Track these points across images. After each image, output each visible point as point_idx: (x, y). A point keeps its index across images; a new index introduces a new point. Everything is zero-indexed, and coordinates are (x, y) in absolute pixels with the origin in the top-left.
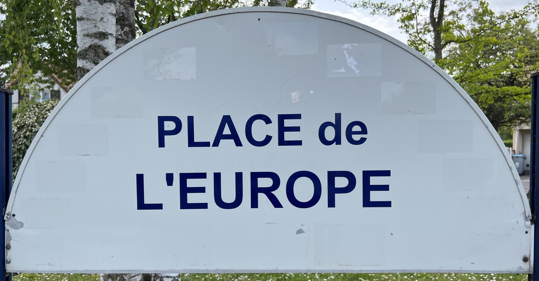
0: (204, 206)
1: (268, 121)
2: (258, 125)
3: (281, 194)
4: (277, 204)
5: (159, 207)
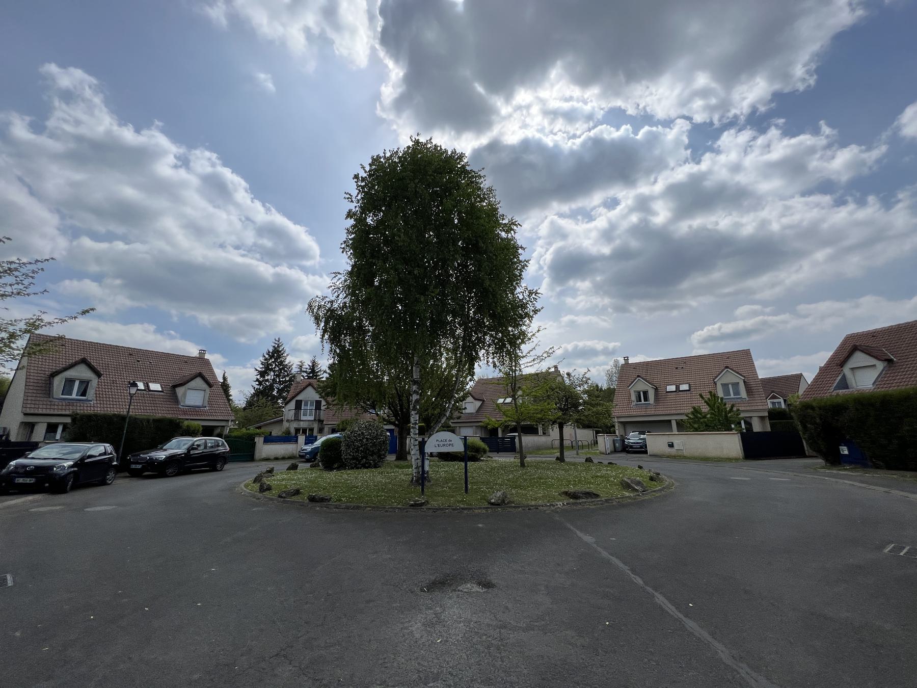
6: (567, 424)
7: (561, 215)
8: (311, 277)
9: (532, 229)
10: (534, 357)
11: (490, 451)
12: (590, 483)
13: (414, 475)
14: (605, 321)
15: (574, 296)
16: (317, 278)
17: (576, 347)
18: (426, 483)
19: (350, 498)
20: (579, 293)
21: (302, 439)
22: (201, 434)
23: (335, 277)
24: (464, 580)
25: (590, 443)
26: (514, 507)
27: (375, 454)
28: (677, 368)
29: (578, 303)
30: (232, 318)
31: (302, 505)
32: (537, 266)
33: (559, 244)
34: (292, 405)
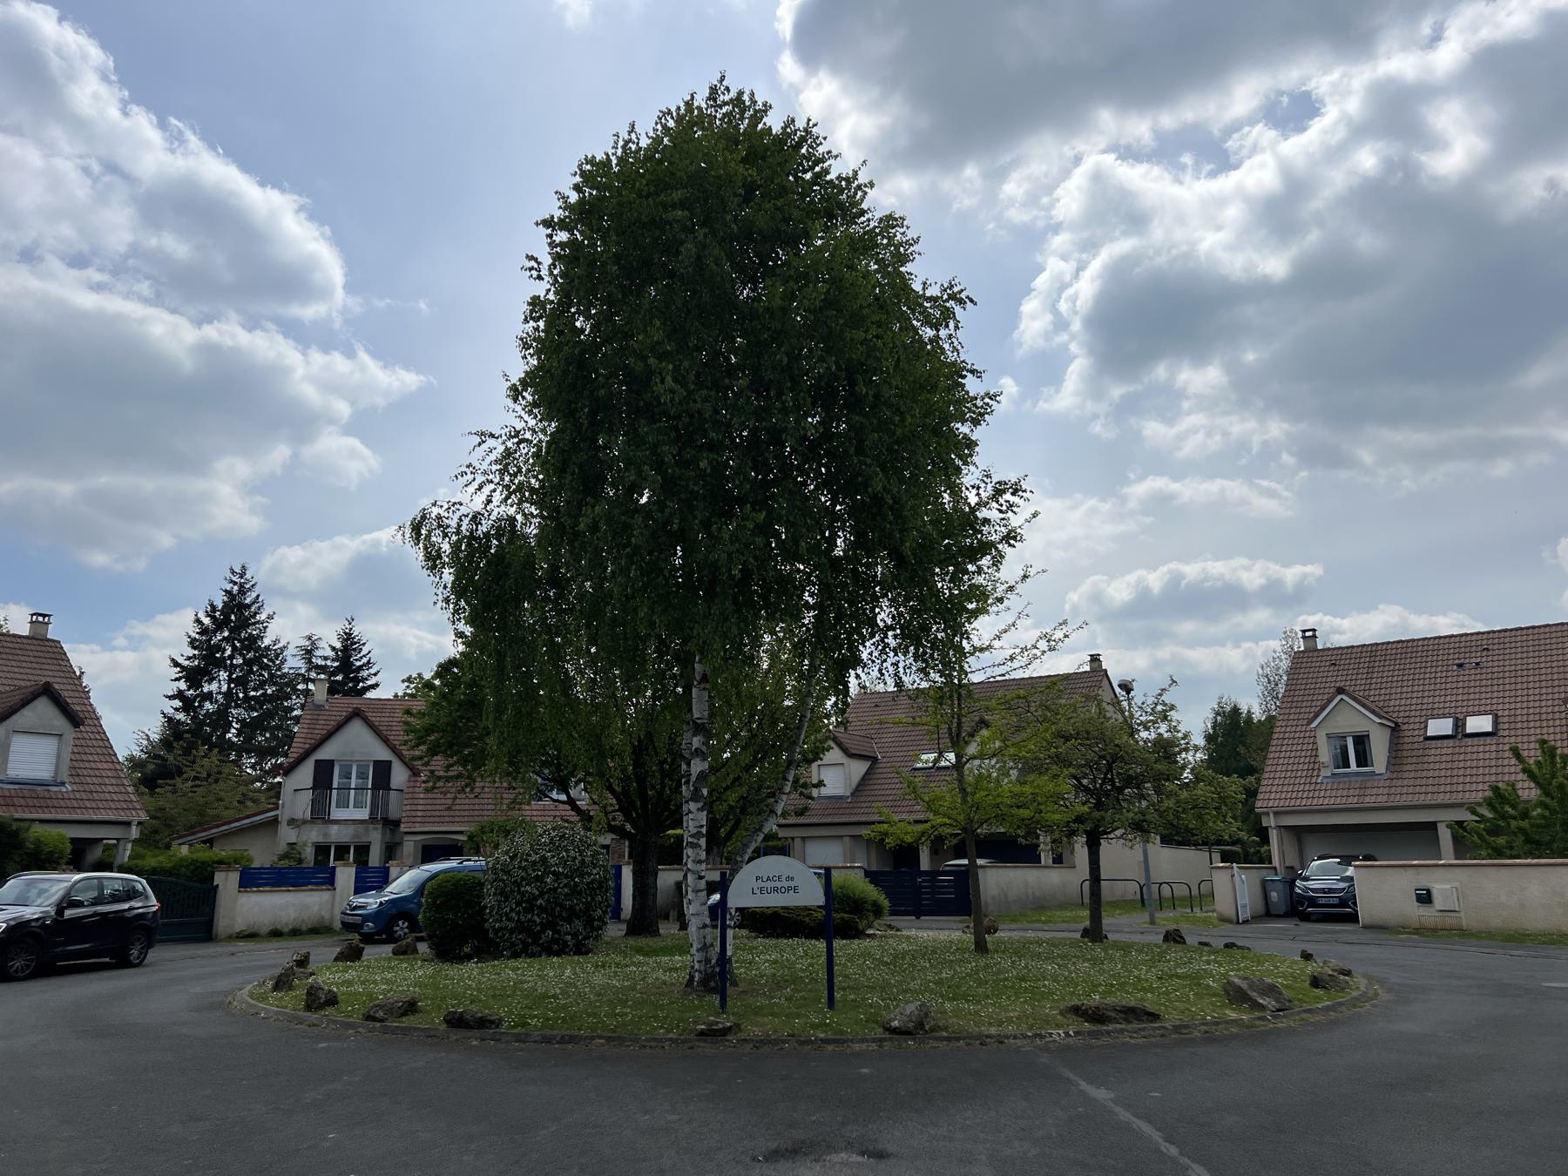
6: (1112, 836)
7: (1129, 153)
8: (317, 358)
9: (1032, 200)
10: (1012, 651)
11: (893, 913)
12: (1151, 990)
13: (697, 966)
14: (1271, 494)
15: (1169, 415)
16: (339, 363)
17: (1175, 580)
18: (730, 991)
19: (548, 1019)
20: (1186, 405)
21: (346, 875)
22: (67, 863)
23: (480, 445)
24: (832, 1148)
25: (1195, 892)
26: (948, 1039)
27: (579, 918)
28: (1460, 666)
29: (1182, 438)
30: (65, 489)
31: (430, 1034)
32: (1049, 317)
33: (1123, 246)
34: (305, 775)
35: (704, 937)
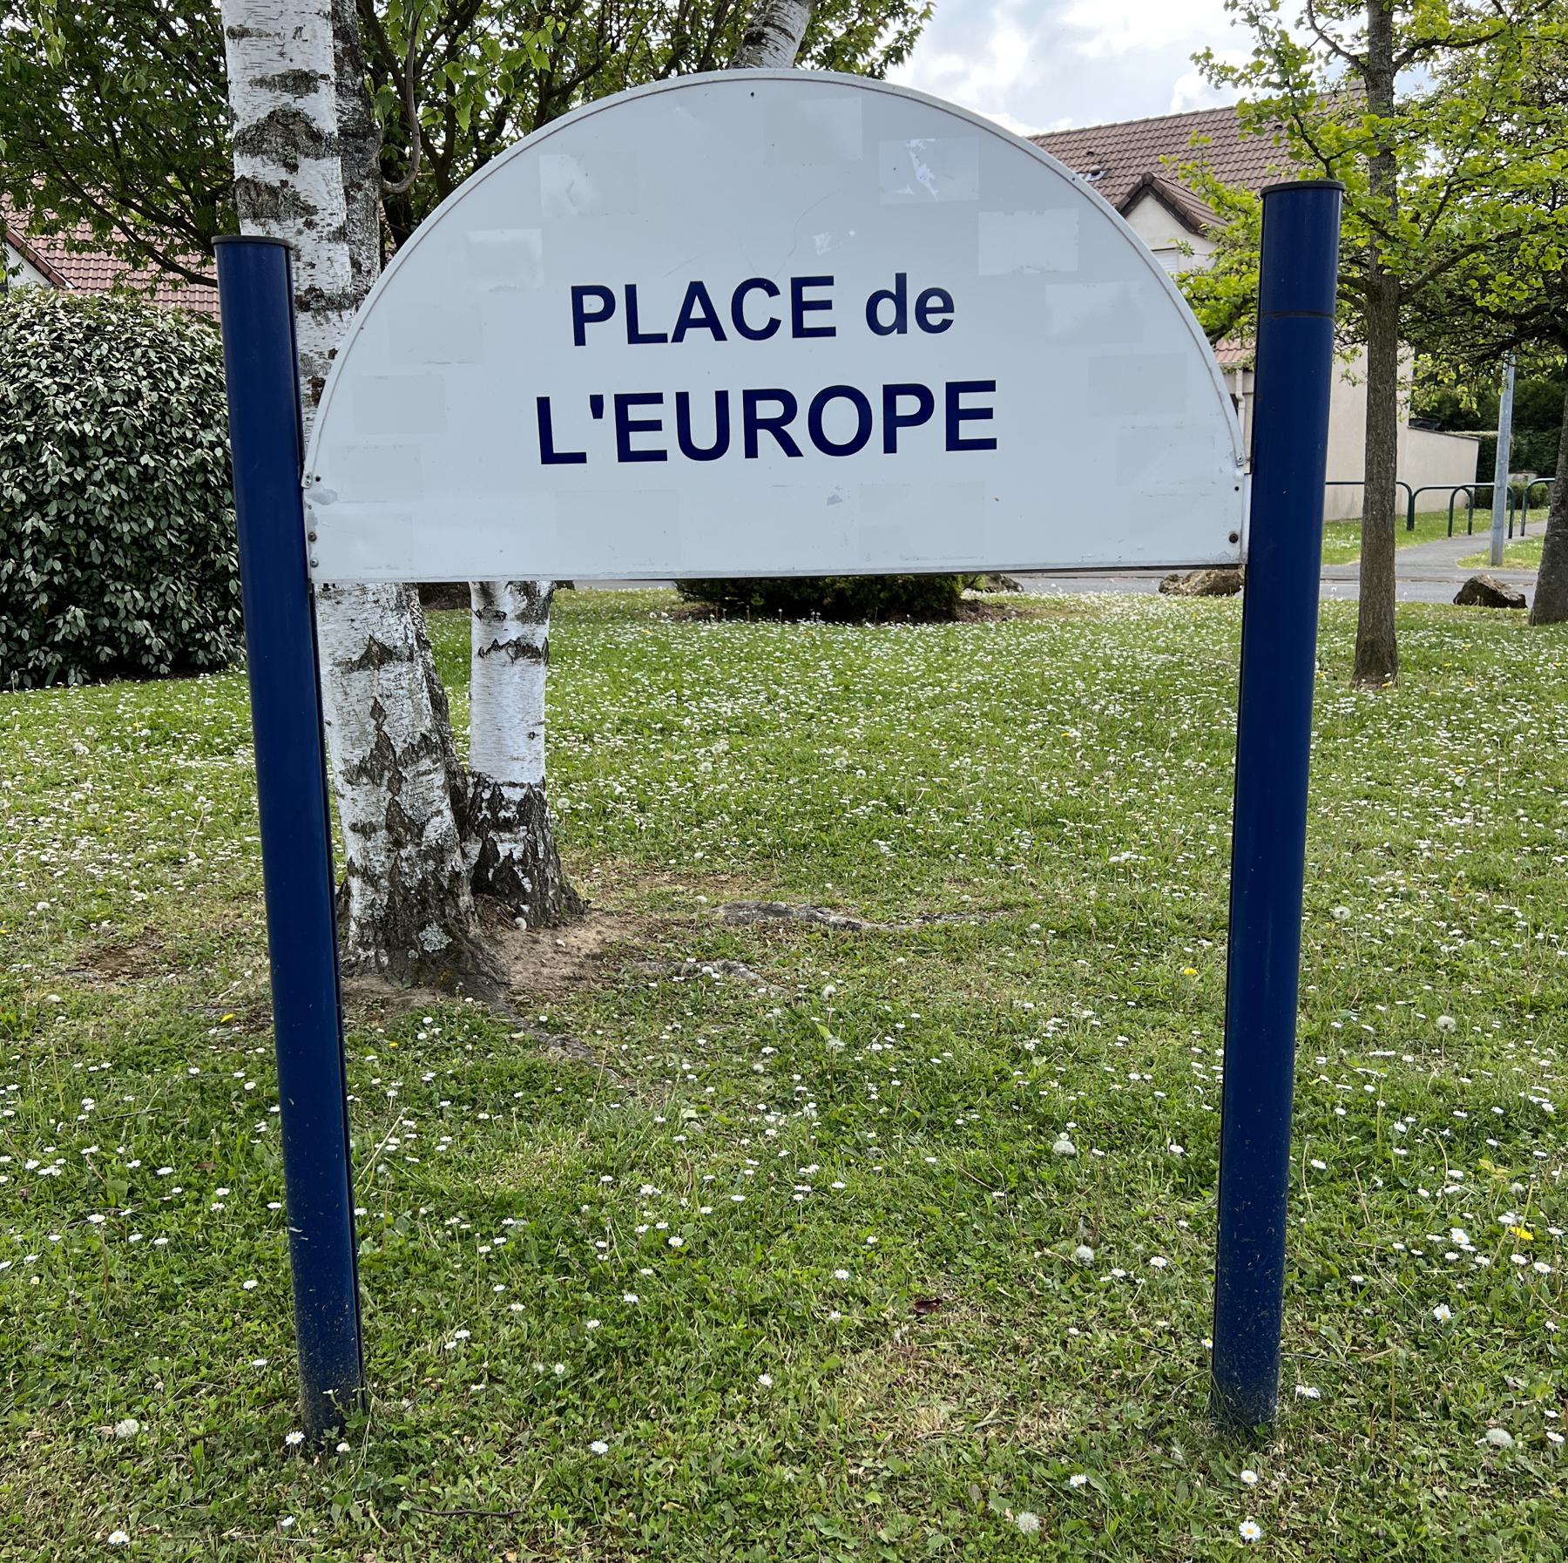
0: (660, 456)
1: (772, 290)
2: (755, 297)
3: (798, 430)
4: (792, 449)
5: (580, 458)
35: (377, 711)
